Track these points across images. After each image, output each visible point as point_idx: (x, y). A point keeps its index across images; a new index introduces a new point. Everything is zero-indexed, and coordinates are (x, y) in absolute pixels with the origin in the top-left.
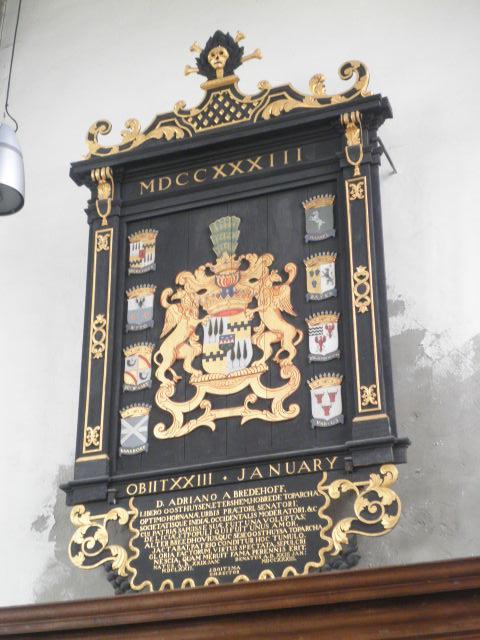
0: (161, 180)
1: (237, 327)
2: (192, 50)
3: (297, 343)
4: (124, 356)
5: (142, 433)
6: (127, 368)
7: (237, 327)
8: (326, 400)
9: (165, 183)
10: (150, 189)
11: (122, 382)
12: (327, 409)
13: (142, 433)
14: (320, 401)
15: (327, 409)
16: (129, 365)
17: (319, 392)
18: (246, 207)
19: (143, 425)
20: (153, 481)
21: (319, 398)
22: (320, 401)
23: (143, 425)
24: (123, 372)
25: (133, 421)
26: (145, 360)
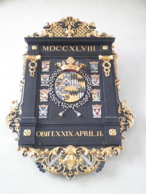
0: (51, 47)
1: (48, 65)
2: (13, 103)
3: (128, 126)
4: (39, 92)
5: (46, 113)
6: (41, 95)
7: (48, 65)
8: (97, 111)
9: (53, 48)
10: (47, 50)
11: (40, 99)
12: (97, 114)
13: (46, 113)
14: (95, 111)
15: (97, 114)
16: (41, 94)
17: (95, 108)
18: (51, 59)
19: (46, 111)
20: (48, 131)
21: (95, 110)
22: (95, 111)
23: (46, 111)
24: (39, 96)
25: (43, 109)
26: (47, 93)
